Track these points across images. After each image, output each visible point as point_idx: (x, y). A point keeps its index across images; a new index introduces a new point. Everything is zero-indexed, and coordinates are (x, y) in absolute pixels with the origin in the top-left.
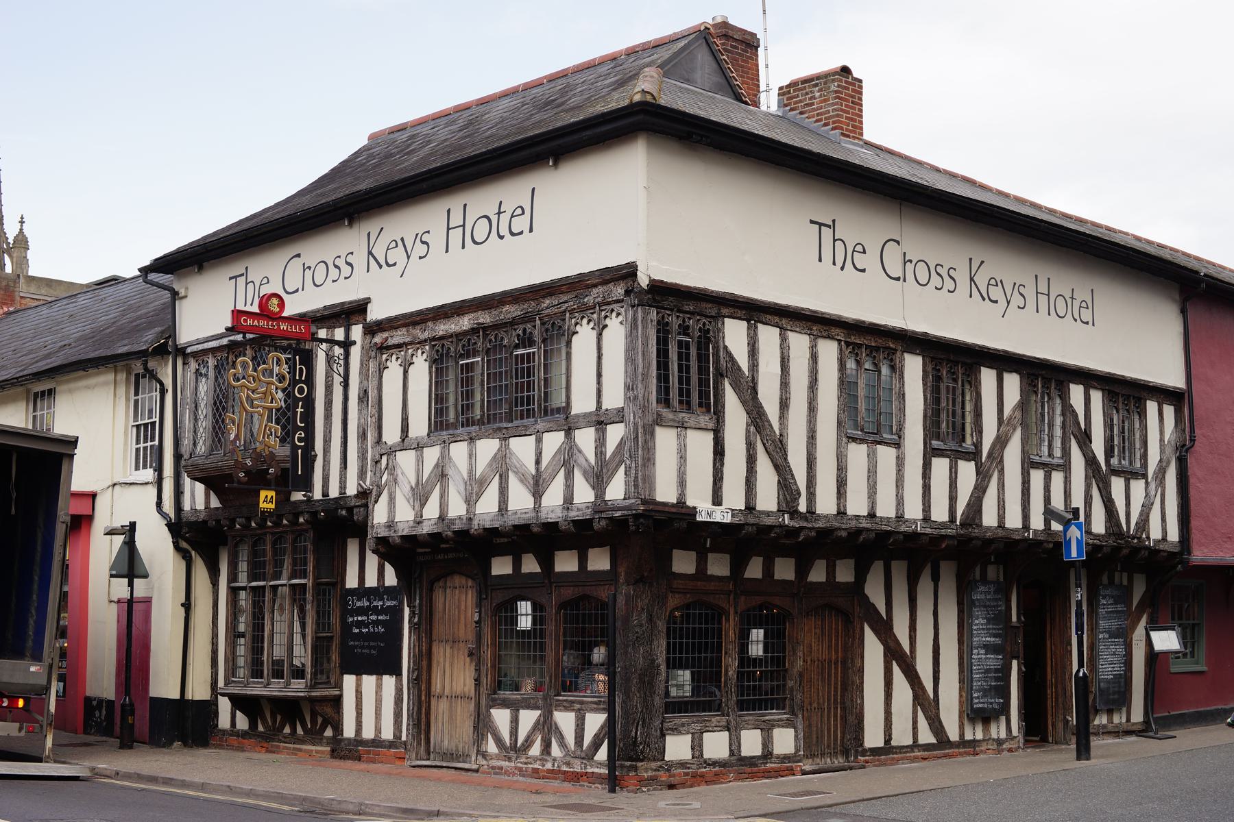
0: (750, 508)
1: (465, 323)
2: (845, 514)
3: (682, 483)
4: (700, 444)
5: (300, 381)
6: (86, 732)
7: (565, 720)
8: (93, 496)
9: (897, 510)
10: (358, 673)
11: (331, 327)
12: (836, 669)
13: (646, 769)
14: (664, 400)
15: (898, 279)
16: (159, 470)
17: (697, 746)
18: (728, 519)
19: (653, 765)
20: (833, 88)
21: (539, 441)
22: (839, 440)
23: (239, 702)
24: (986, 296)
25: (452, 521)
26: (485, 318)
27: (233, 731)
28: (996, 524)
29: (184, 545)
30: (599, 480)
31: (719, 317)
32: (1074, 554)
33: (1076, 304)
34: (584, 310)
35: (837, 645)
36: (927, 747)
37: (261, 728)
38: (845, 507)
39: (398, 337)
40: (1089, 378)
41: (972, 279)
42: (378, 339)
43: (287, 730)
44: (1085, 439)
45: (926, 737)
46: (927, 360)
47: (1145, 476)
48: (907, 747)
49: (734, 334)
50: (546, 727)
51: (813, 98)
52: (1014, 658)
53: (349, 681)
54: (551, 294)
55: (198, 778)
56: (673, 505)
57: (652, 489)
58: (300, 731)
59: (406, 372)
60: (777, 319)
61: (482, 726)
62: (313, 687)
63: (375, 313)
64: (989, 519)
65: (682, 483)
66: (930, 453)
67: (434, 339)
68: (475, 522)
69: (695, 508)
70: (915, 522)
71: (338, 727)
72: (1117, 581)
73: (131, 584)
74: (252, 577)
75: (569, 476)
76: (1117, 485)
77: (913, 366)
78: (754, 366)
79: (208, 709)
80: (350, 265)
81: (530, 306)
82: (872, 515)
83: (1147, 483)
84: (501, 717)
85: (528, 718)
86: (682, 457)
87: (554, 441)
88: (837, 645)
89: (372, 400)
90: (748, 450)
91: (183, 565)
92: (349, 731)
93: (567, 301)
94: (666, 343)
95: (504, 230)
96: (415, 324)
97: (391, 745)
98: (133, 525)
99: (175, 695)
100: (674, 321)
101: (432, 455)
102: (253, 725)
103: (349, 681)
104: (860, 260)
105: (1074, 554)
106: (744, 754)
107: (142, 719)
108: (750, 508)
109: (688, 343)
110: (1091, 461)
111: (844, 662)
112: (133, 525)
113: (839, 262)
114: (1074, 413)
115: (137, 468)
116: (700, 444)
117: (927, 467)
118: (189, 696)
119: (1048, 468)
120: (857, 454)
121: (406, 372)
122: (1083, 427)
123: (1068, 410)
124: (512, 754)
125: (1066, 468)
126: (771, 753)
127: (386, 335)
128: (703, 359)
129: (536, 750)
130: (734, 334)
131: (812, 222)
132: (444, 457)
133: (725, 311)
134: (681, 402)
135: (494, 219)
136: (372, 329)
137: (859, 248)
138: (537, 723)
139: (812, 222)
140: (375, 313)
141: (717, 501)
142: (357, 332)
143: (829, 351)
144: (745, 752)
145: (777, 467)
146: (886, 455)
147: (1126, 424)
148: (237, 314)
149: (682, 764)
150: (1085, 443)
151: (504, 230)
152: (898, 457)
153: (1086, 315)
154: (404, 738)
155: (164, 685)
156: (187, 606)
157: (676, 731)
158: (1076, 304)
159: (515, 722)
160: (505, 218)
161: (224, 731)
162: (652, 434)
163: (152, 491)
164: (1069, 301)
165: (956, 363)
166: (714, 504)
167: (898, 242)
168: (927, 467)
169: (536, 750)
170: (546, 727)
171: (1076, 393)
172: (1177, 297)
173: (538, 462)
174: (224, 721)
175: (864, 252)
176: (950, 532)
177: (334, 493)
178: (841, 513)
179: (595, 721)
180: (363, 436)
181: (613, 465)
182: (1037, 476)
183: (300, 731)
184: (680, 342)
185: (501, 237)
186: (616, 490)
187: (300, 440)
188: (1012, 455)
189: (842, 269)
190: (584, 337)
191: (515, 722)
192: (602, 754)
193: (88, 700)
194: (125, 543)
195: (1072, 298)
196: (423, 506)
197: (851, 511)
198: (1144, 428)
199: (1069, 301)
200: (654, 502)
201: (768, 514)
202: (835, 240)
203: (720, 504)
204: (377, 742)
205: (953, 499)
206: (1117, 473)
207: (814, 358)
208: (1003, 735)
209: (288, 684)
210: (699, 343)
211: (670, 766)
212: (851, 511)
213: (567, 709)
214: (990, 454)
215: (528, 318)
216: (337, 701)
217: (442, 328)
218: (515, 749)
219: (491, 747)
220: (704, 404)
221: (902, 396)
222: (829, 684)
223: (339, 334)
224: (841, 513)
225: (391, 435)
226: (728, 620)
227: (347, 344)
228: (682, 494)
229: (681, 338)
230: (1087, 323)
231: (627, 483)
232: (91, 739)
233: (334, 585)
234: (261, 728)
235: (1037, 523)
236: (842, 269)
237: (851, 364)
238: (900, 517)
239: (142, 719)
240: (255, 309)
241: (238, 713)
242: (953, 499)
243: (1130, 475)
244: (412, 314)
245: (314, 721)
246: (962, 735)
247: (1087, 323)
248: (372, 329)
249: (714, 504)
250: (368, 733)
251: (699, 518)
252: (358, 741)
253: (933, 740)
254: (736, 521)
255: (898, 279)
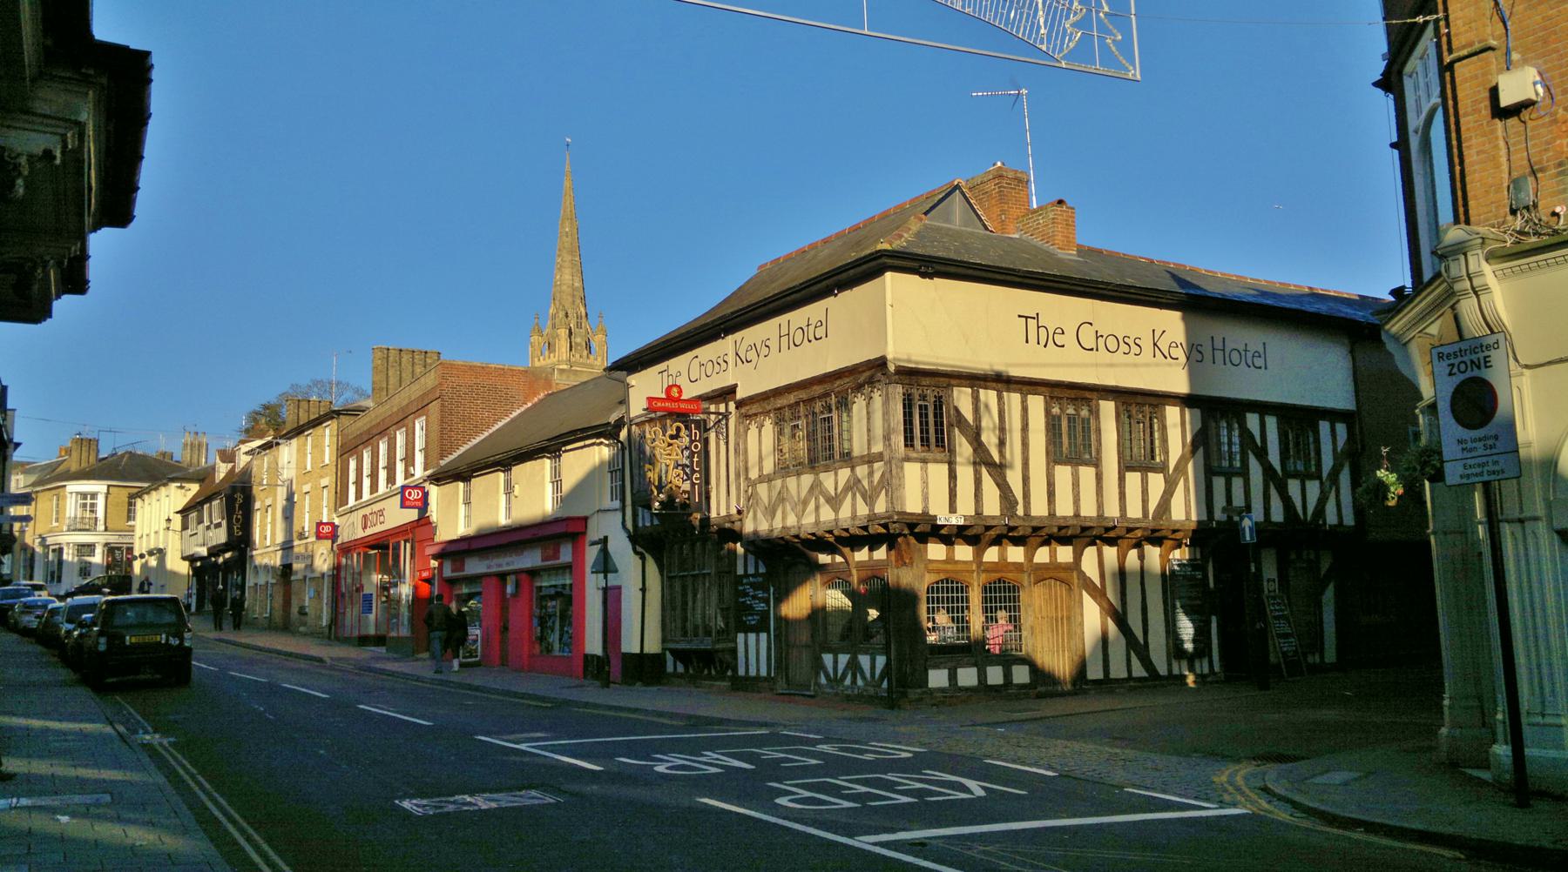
0: (978, 513)
1: (792, 398)
2: (1055, 515)
3: (926, 498)
4: (939, 472)
5: (695, 441)
6: (585, 677)
7: (864, 660)
8: (585, 519)
9: (1098, 511)
10: (746, 632)
11: (717, 403)
12: (1062, 623)
13: (914, 693)
14: (909, 441)
15: (1092, 349)
16: (623, 501)
17: (953, 677)
18: (961, 522)
19: (919, 691)
20: (1051, 216)
21: (836, 474)
22: (1048, 464)
23: (679, 655)
24: (1167, 355)
25: (789, 529)
26: (803, 395)
27: (675, 674)
28: (1184, 518)
29: (639, 549)
30: (870, 499)
31: (949, 386)
32: (1248, 538)
33: (1249, 355)
34: (859, 388)
35: (1062, 606)
36: (1140, 679)
37: (691, 671)
38: (1055, 510)
39: (754, 409)
40: (1263, 408)
41: (1155, 344)
42: (743, 410)
43: (706, 672)
44: (1262, 454)
45: (1139, 670)
46: (1120, 404)
47: (1319, 477)
48: (1123, 679)
49: (962, 399)
50: (854, 666)
51: (1039, 224)
52: (1212, 614)
53: (741, 637)
54: (840, 378)
55: (632, 704)
56: (919, 515)
57: (903, 504)
58: (713, 672)
59: (760, 431)
60: (994, 385)
61: (818, 666)
62: (714, 643)
63: (741, 394)
64: (1331, 518)
65: (926, 498)
66: (1126, 467)
67: (775, 409)
68: (802, 530)
69: (936, 516)
70: (1113, 519)
71: (735, 669)
72: (1305, 557)
73: (606, 577)
74: (681, 569)
75: (817, 499)
76: (1294, 487)
77: (1108, 408)
78: (977, 417)
79: (658, 659)
80: (725, 362)
81: (827, 387)
82: (1077, 515)
83: (1322, 483)
84: (828, 659)
85: (844, 659)
86: (925, 483)
87: (844, 474)
88: (1062, 606)
89: (742, 451)
90: (975, 475)
91: (640, 561)
92: (741, 672)
93: (846, 382)
94: (910, 406)
95: (811, 338)
96: (764, 400)
97: (765, 679)
98: (606, 538)
99: (637, 650)
100: (916, 393)
101: (778, 483)
102: (686, 668)
103: (741, 637)
104: (1059, 339)
105: (1248, 538)
106: (989, 683)
107: (615, 668)
108: (978, 513)
109: (926, 406)
110: (1268, 470)
111: (1069, 618)
112: (606, 538)
113: (1043, 342)
114: (1252, 436)
115: (612, 500)
116: (939, 472)
117: (1122, 479)
118: (646, 650)
119: (1229, 475)
120: (1063, 473)
121: (760, 431)
122: (1259, 444)
123: (1246, 434)
124: (834, 684)
125: (1244, 473)
126: (1011, 683)
127: (748, 408)
128: (938, 415)
129: (848, 682)
130: (962, 399)
131: (1020, 316)
132: (784, 486)
133: (953, 382)
134: (937, 446)
135: (805, 329)
136: (739, 405)
137: (1059, 331)
138: (849, 663)
139: (1020, 316)
140: (741, 394)
141: (953, 509)
142: (732, 406)
143: (1037, 403)
144: (990, 682)
145: (998, 485)
146: (1087, 473)
147: (1301, 439)
148: (650, 399)
149: (942, 690)
150: (1261, 456)
151: (811, 338)
152: (1097, 474)
153: (1259, 362)
154: (773, 675)
155: (630, 645)
156: (643, 590)
157: (936, 667)
158: (1249, 355)
159: (836, 662)
160: (811, 328)
161: (669, 674)
162: (902, 468)
163: (619, 515)
164: (1243, 353)
165: (1144, 405)
166: (950, 512)
167: (1091, 324)
168: (1122, 479)
169: (848, 682)
170: (854, 666)
171: (1252, 421)
172: (1346, 341)
173: (836, 489)
174: (670, 669)
175: (1063, 333)
176: (1143, 525)
177: (723, 513)
178: (1052, 514)
179: (881, 661)
180: (738, 475)
181: (878, 490)
182: (1219, 483)
183: (713, 672)
184: (920, 406)
185: (810, 341)
186: (881, 507)
187: (696, 479)
188: (1345, 478)
189: (1045, 346)
190: (859, 405)
191: (836, 662)
192: (885, 684)
193: (586, 656)
194: (601, 550)
195: (1246, 351)
196: (772, 519)
197: (1059, 513)
198: (1317, 441)
199: (1243, 353)
200: (905, 513)
201: (993, 518)
202: (1038, 327)
203: (955, 512)
204: (758, 678)
205: (1145, 502)
206: (1295, 475)
207: (1025, 409)
208: (1206, 670)
209: (702, 642)
210: (935, 406)
211: (932, 691)
212: (1059, 513)
213: (866, 653)
214: (1176, 468)
215: (827, 395)
216: (734, 651)
217: (780, 402)
218: (835, 681)
219: (823, 680)
220: (940, 442)
221: (1099, 431)
222: (1057, 634)
223: (722, 408)
224: (1052, 514)
225: (754, 474)
226: (973, 590)
227: (726, 416)
228: (926, 507)
229: (920, 403)
230: (1260, 368)
231: (887, 502)
232: (586, 682)
233: (729, 572)
234: (691, 671)
235: (1219, 515)
236: (1045, 346)
237: (1056, 410)
238: (1100, 516)
239: (615, 668)
240: (663, 396)
241: (678, 663)
242: (1145, 502)
243: (1304, 477)
244: (762, 394)
245: (721, 668)
246: (1170, 670)
247: (1260, 368)
248: (739, 405)
249: (950, 512)
250: (753, 673)
251: (939, 523)
252: (747, 678)
253: (1145, 674)
254: (968, 523)
255: (1092, 349)
